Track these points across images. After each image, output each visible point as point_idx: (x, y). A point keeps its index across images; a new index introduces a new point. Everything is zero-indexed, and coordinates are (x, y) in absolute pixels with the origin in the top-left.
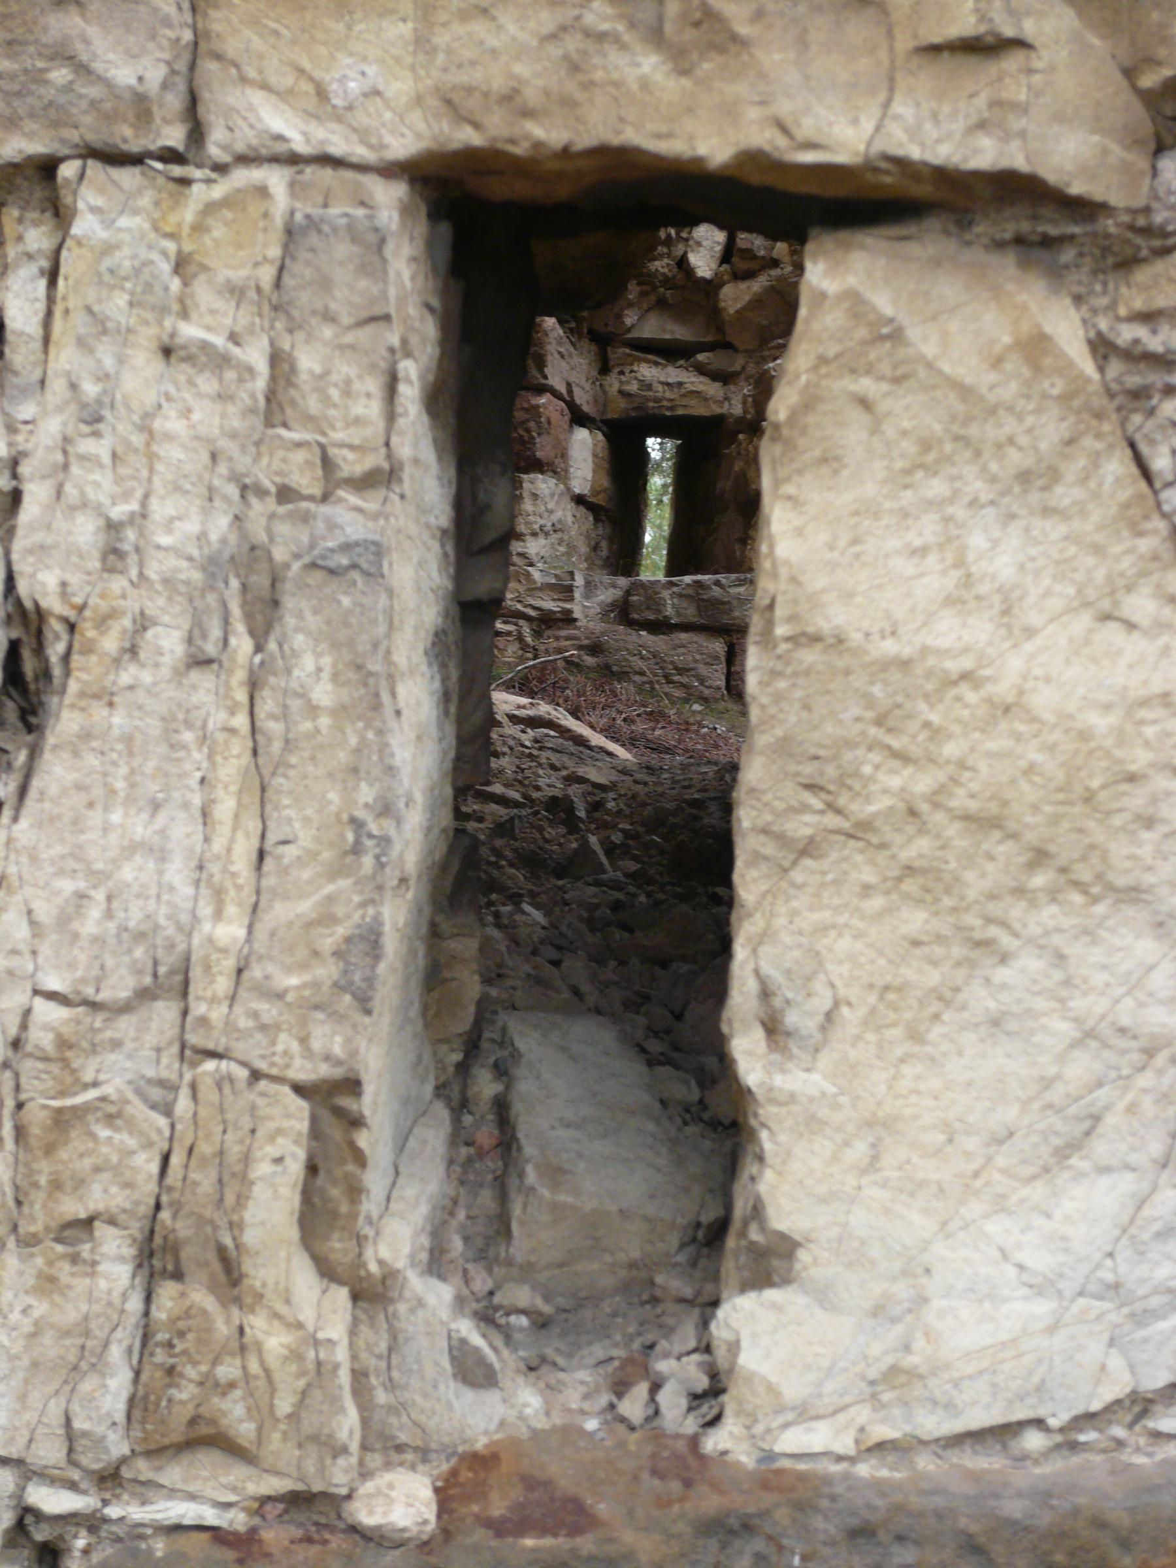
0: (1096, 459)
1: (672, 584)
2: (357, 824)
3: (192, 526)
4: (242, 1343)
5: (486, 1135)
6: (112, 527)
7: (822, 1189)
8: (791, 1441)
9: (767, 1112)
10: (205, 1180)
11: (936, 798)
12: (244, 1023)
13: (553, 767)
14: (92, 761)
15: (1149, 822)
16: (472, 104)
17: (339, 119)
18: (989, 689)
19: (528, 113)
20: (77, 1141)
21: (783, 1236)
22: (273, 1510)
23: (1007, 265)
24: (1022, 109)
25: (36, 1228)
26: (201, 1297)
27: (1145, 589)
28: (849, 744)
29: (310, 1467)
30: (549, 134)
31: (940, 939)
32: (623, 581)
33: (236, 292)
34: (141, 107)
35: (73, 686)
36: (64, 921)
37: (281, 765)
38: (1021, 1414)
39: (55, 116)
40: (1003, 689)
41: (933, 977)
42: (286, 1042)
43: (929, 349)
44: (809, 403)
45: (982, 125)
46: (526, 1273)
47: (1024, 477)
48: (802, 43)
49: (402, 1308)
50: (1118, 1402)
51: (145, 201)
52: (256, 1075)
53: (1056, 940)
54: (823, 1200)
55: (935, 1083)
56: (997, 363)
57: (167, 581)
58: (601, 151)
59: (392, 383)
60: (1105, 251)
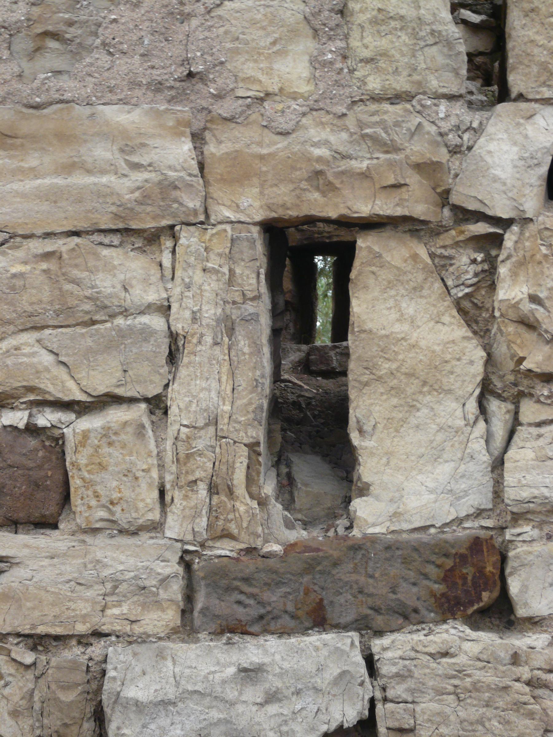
0: (432, 283)
1: (335, 347)
2: (256, 380)
3: (213, 312)
4: (234, 509)
5: (285, 482)
6: (193, 312)
7: (375, 471)
8: (371, 531)
9: (360, 452)
10: (224, 468)
11: (398, 369)
12: (232, 429)
13: (292, 393)
14: (191, 369)
15: (452, 373)
16: (274, 207)
17: (242, 212)
18: (409, 341)
19: (288, 209)
20: (192, 461)
21: (366, 483)
22: (243, 553)
23: (407, 236)
24: (406, 200)
25: (183, 484)
26: (224, 498)
27: (447, 315)
28: (375, 357)
29: (252, 541)
30: (293, 213)
31: (401, 405)
32: (304, 347)
33: (220, 255)
34: (195, 212)
35: (186, 351)
36: (186, 408)
37: (237, 368)
38: (428, 523)
39: (174, 215)
40: (412, 341)
41: (401, 415)
42: (242, 434)
43: (388, 259)
44: (360, 274)
45: (397, 205)
46: (300, 511)
47: (415, 289)
48: (353, 188)
49: (270, 507)
50: (453, 520)
51: (196, 234)
52: (235, 442)
53: (431, 404)
54: (376, 473)
55: (403, 443)
56: (406, 261)
57: (207, 325)
58: (306, 216)
59: (258, 274)
60: (432, 232)
